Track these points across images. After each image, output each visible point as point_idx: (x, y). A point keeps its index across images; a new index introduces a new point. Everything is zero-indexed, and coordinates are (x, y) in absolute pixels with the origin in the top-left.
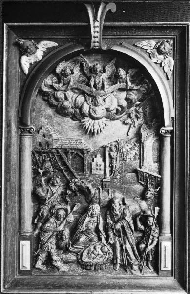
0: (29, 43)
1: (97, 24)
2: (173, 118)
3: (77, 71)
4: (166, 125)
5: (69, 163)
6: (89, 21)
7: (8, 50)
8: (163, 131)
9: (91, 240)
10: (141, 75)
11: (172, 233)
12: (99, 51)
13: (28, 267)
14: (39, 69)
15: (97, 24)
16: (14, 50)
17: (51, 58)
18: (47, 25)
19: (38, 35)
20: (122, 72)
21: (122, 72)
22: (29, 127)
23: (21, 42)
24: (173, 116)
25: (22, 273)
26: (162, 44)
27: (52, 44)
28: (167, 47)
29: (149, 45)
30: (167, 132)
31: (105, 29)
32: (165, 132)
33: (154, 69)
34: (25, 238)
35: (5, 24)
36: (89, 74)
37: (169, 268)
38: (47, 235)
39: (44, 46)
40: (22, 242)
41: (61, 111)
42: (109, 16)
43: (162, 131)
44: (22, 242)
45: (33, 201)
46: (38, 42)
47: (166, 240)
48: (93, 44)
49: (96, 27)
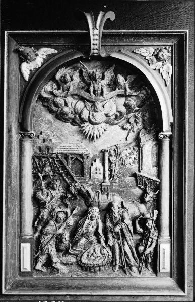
0: (29, 50)
1: (96, 32)
2: (171, 123)
3: (76, 78)
4: (164, 130)
5: (69, 167)
6: (88, 29)
7: (8, 56)
8: (162, 136)
9: (91, 243)
10: (140, 82)
11: (170, 235)
12: (98, 58)
13: (29, 269)
14: (39, 76)
15: (96, 32)
16: (14, 57)
17: (50, 66)
18: (47, 33)
19: (38, 42)
20: (121, 79)
21: (121, 79)
22: (29, 133)
23: (22, 49)
24: (172, 121)
25: (23, 274)
26: (160, 51)
27: (52, 51)
28: (166, 54)
29: (148, 51)
30: (165, 136)
31: (105, 36)
32: (164, 137)
33: (153, 76)
34: (25, 241)
35: (6, 32)
36: (88, 81)
37: (168, 270)
38: (48, 238)
39: (44, 53)
40: (22, 245)
41: (61, 116)
42: (108, 24)
43: (161, 135)
44: (22, 245)
45: (34, 205)
46: (38, 50)
47: (166, 242)
48: (92, 51)
49: (95, 35)
